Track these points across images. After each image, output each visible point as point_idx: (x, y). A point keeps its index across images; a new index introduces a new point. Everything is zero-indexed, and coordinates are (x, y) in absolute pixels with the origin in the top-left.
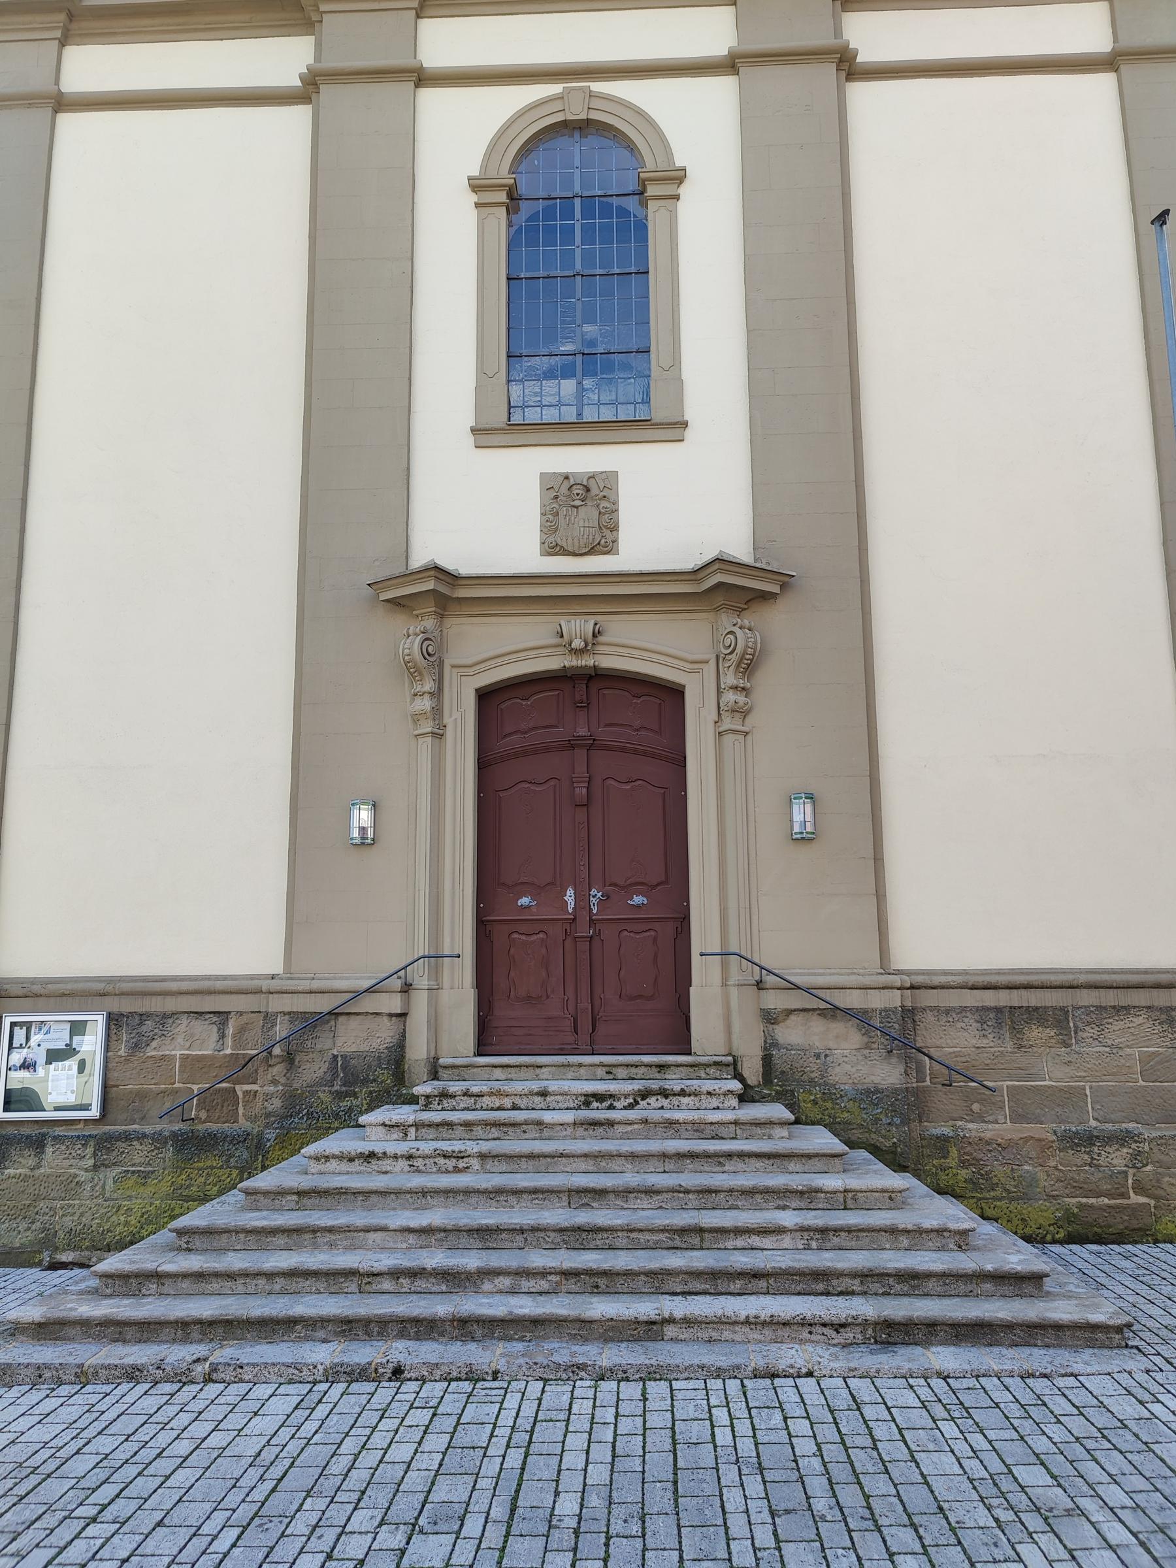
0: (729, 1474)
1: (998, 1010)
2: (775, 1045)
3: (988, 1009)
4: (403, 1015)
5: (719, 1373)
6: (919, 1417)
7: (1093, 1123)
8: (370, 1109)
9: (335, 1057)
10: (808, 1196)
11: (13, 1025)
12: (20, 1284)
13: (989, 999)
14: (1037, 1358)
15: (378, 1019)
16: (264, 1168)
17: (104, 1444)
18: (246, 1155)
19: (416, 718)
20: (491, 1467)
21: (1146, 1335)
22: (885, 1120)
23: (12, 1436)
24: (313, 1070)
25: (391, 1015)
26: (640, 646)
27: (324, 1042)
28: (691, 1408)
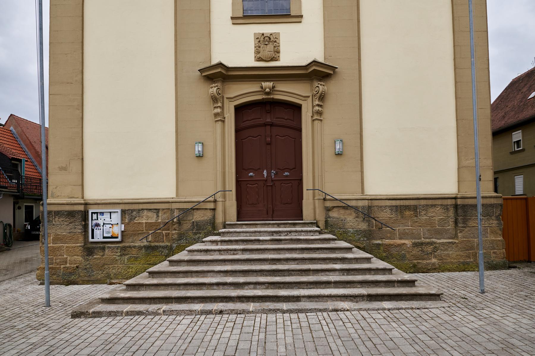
0: (330, 339)
1: (396, 206)
2: (329, 217)
3: (393, 206)
4: (214, 209)
5: (320, 310)
6: (384, 322)
7: (423, 239)
8: (205, 237)
9: (193, 222)
10: (343, 260)
11: (92, 213)
12: (101, 289)
13: (394, 203)
14: (415, 304)
15: (206, 211)
16: (173, 255)
17: (132, 334)
18: (167, 251)
19: (216, 115)
20: (255, 338)
21: (445, 297)
22: (362, 239)
23: (103, 332)
24: (186, 226)
25: (210, 209)
26: (287, 91)
27: (190, 218)
28: (314, 320)
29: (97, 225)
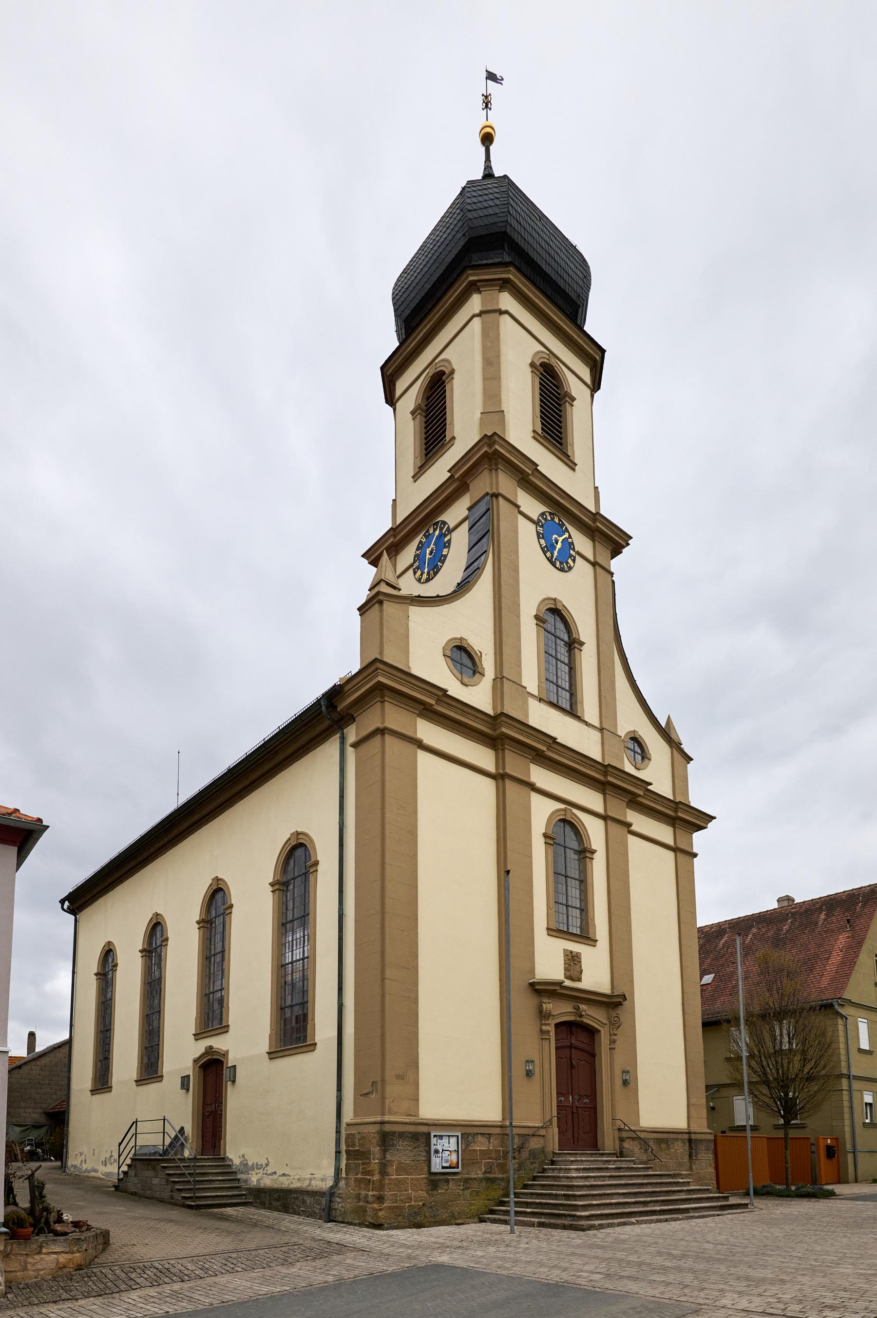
29: (437, 1152)
